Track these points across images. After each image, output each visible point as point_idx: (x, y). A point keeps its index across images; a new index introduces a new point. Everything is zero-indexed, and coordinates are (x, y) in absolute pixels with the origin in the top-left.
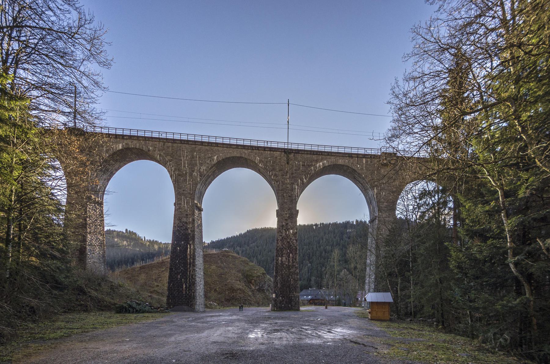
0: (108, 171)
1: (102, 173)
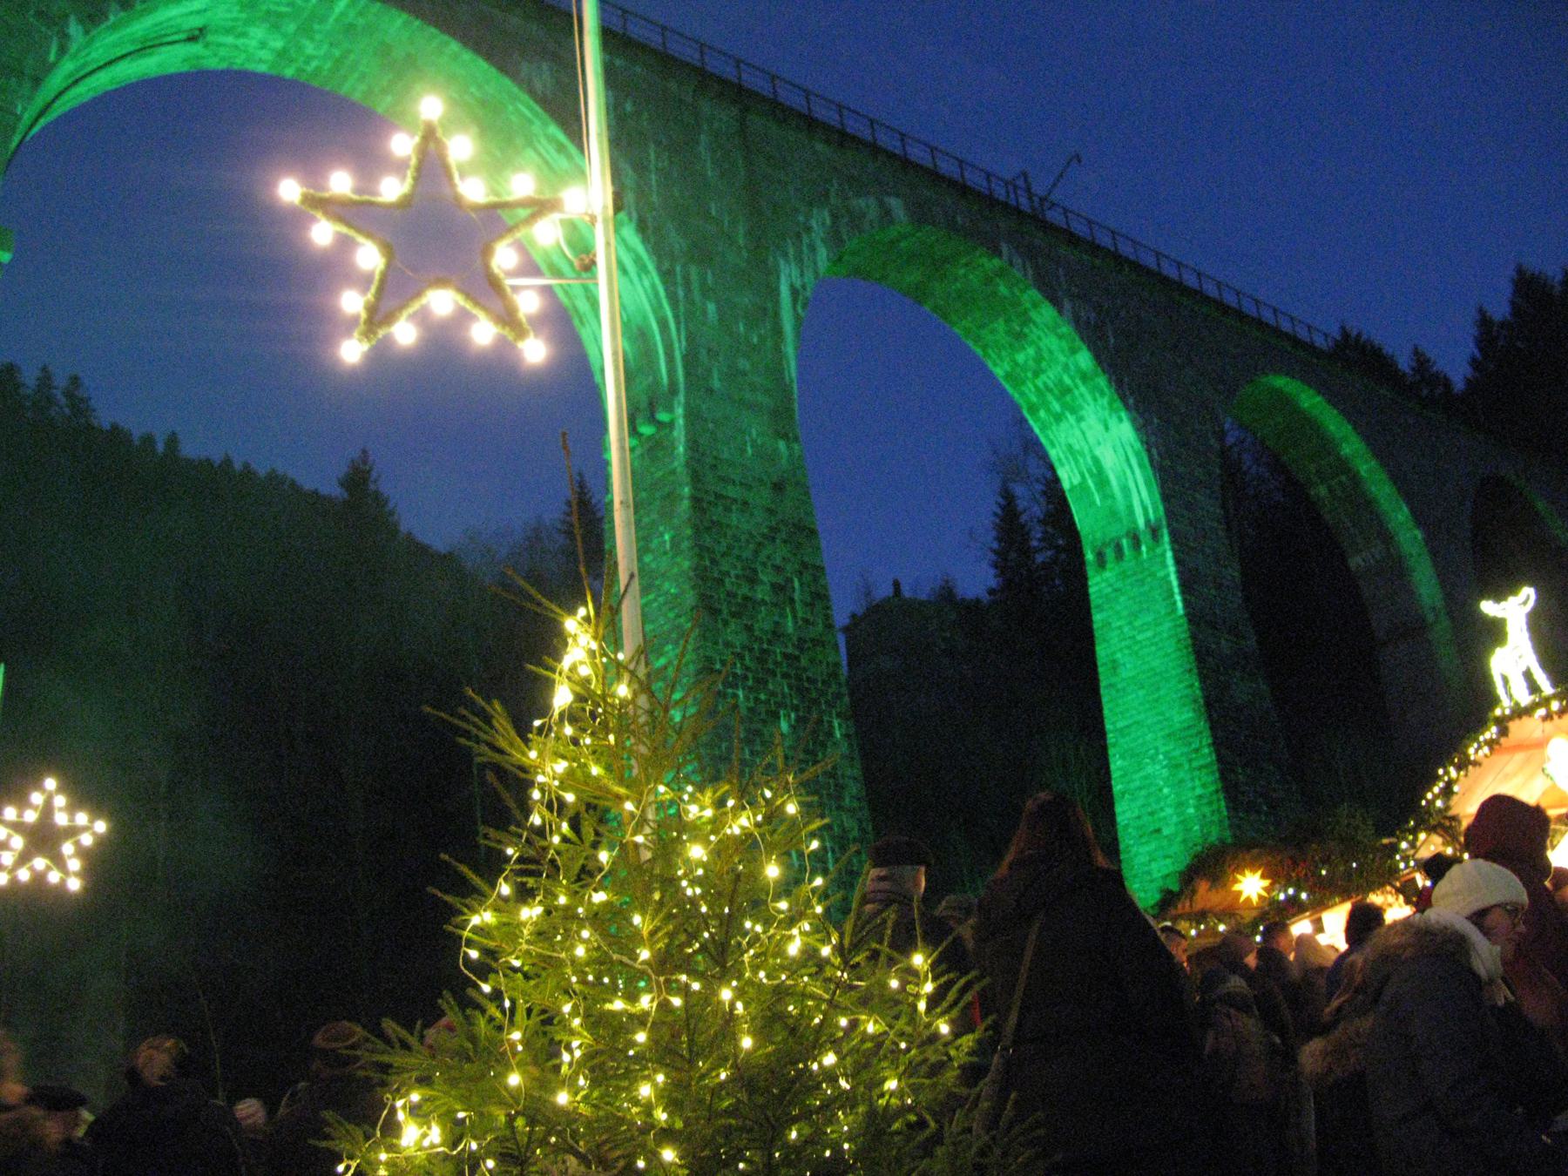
1: (1072, 419)
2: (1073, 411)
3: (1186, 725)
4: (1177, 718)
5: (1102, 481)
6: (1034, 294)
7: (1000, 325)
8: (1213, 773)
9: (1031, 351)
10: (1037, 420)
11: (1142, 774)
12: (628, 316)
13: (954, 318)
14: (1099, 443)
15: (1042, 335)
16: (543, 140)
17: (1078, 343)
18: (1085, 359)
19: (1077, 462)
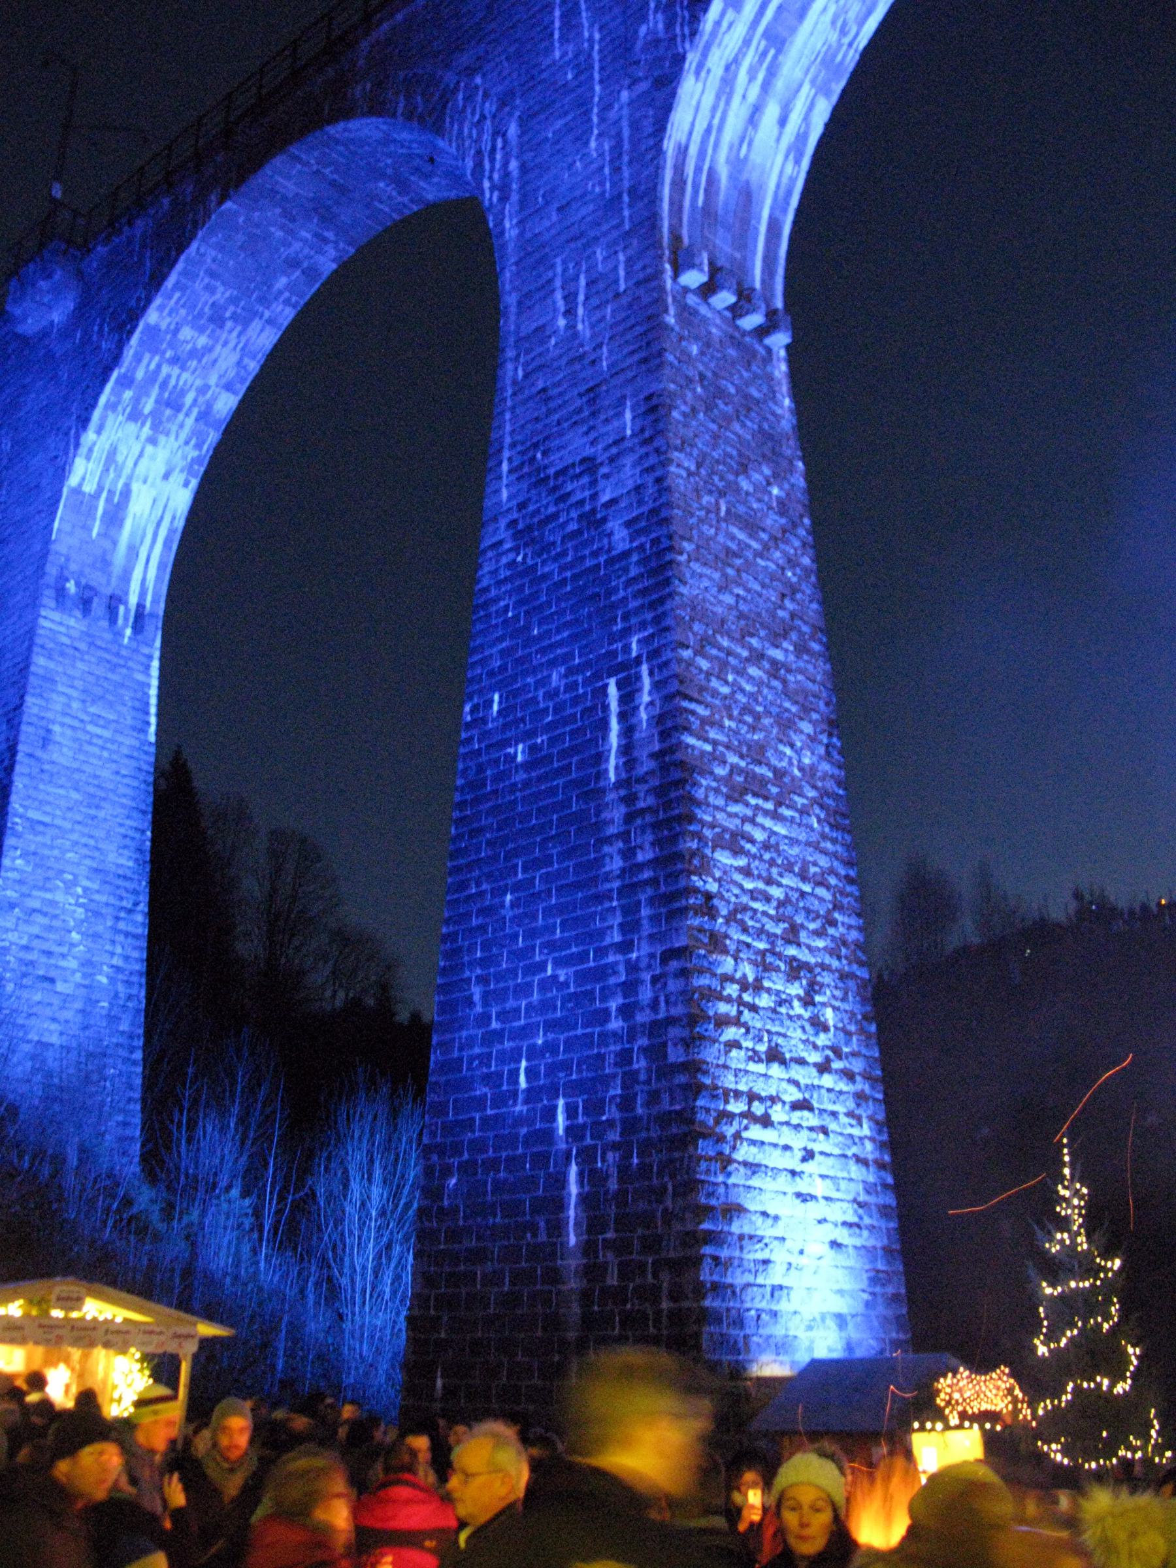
0: (178, 408)
1: (146, 431)
2: (155, 427)
3: (121, 872)
4: (112, 857)
5: (115, 517)
6: (287, 315)
7: (222, 294)
8: (140, 948)
9: (202, 341)
10: (117, 393)
11: (48, 896)
12: (746, 157)
14: (145, 482)
15: (231, 345)
17: (242, 389)
18: (226, 404)
19: (106, 470)
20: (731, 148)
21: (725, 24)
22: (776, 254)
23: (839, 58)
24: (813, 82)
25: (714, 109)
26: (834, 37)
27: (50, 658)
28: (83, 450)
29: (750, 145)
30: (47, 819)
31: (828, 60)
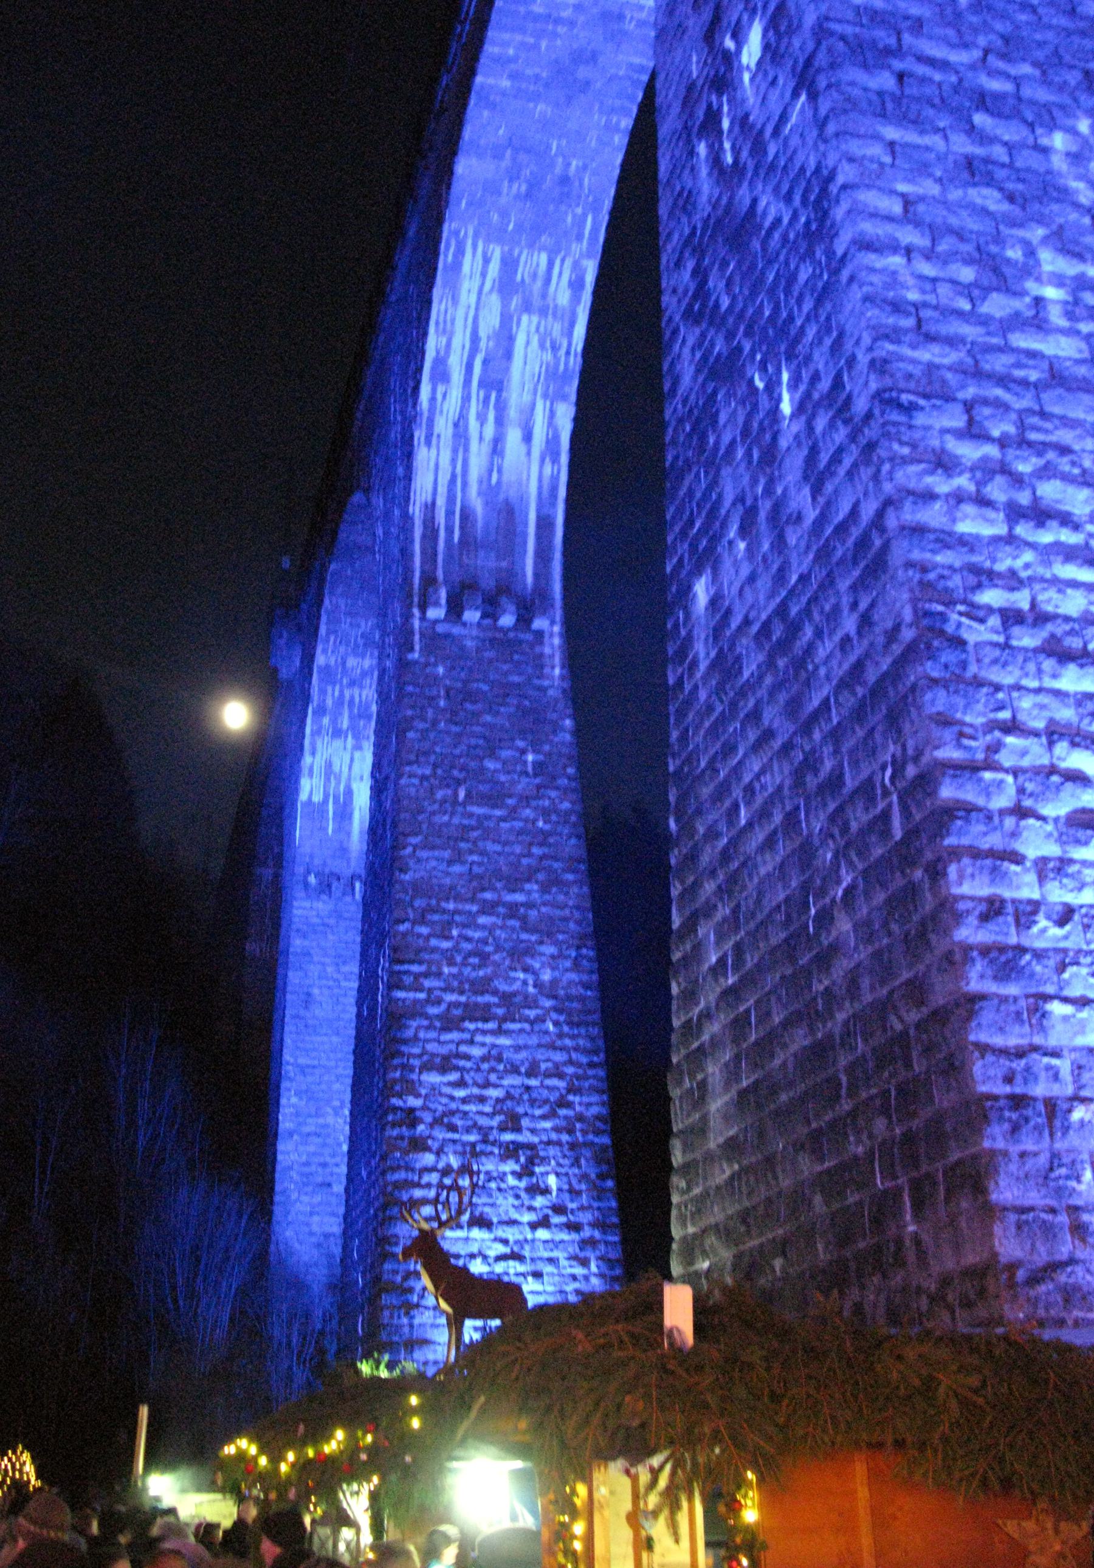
1: (350, 741)
2: (357, 737)
11: (321, 1121)
12: (499, 482)
13: (340, 590)
16: (568, 263)
19: (328, 779)
20: (480, 482)
21: (439, 397)
22: (551, 542)
23: (562, 367)
24: (545, 396)
25: (454, 461)
26: (548, 356)
27: (305, 937)
28: (305, 771)
29: (500, 471)
30: (316, 1062)
31: (552, 374)
